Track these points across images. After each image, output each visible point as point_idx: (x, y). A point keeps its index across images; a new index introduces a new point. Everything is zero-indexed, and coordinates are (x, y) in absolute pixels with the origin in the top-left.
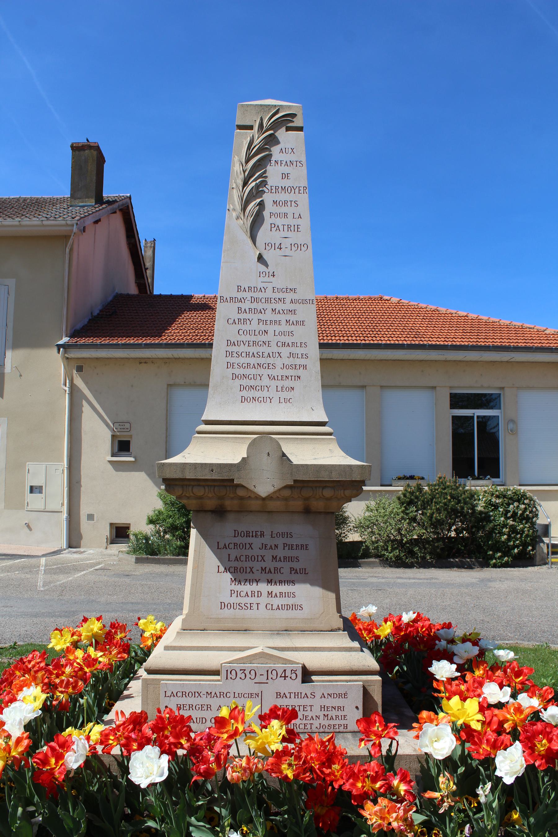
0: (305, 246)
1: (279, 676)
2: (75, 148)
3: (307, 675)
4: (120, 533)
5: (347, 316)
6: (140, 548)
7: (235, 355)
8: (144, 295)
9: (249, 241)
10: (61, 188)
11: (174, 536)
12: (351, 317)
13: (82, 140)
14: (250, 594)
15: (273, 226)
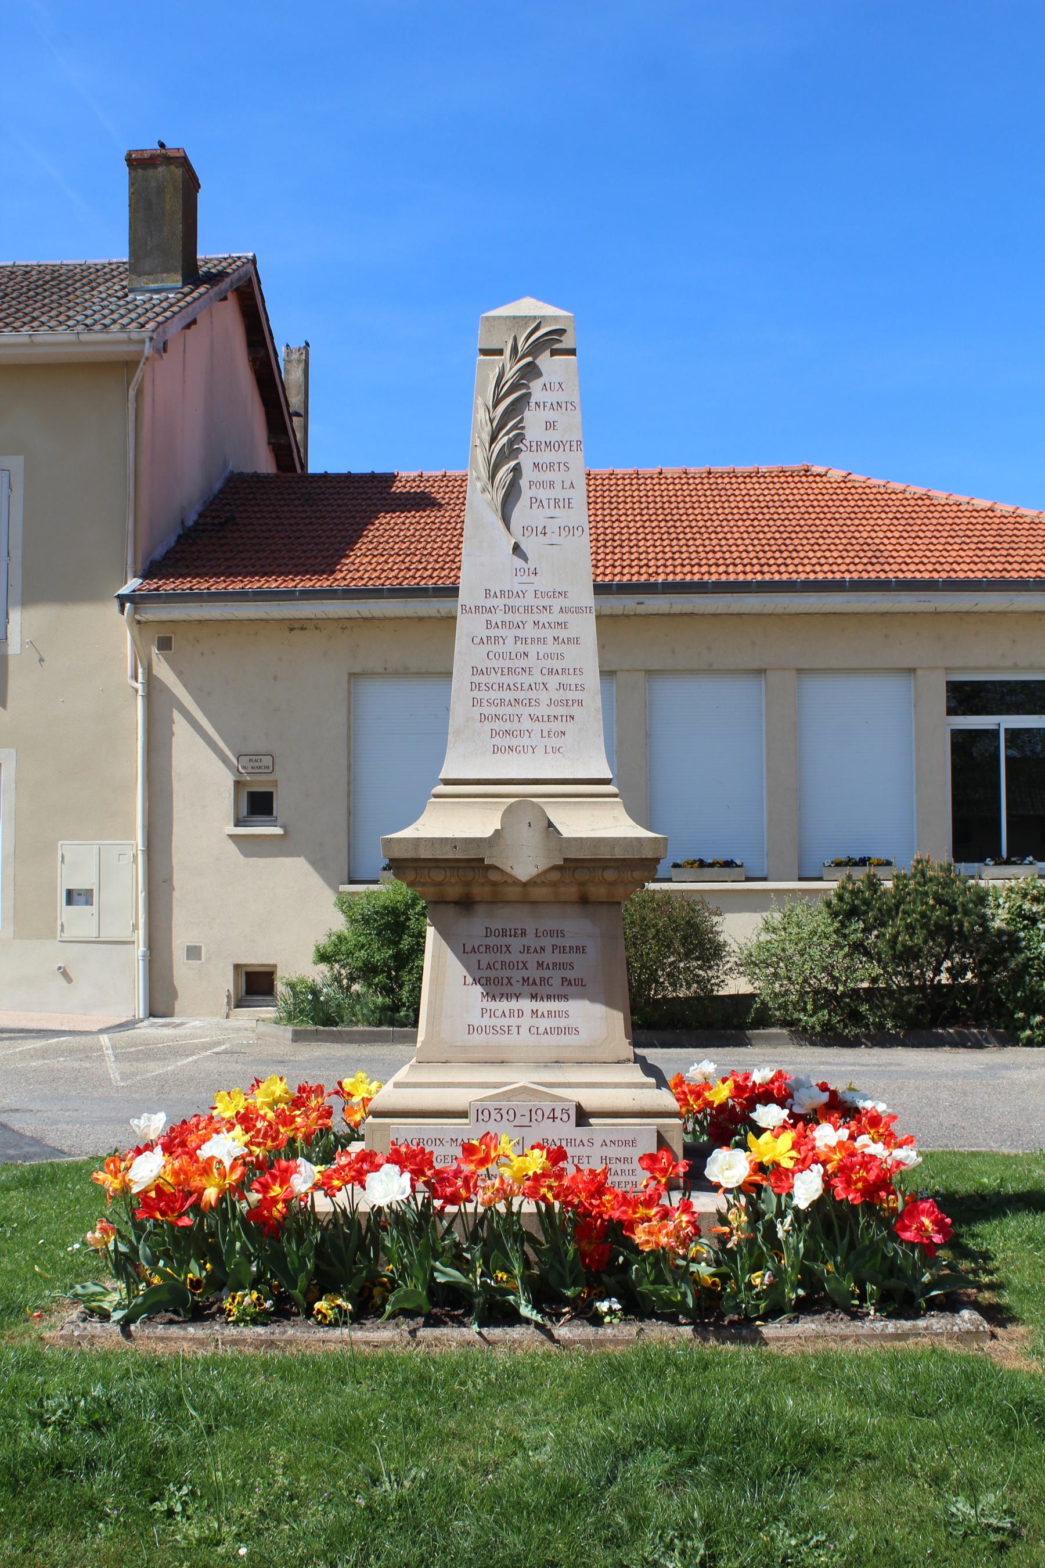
0: (580, 529)
1: (546, 1116)
2: (136, 163)
3: (583, 1116)
4: (256, 984)
5: (730, 517)
6: (301, 1011)
7: (483, 687)
8: (289, 474)
9: (501, 524)
10: (109, 243)
11: (370, 986)
12: (737, 517)
13: (149, 144)
14: (507, 1014)
15: (534, 500)
